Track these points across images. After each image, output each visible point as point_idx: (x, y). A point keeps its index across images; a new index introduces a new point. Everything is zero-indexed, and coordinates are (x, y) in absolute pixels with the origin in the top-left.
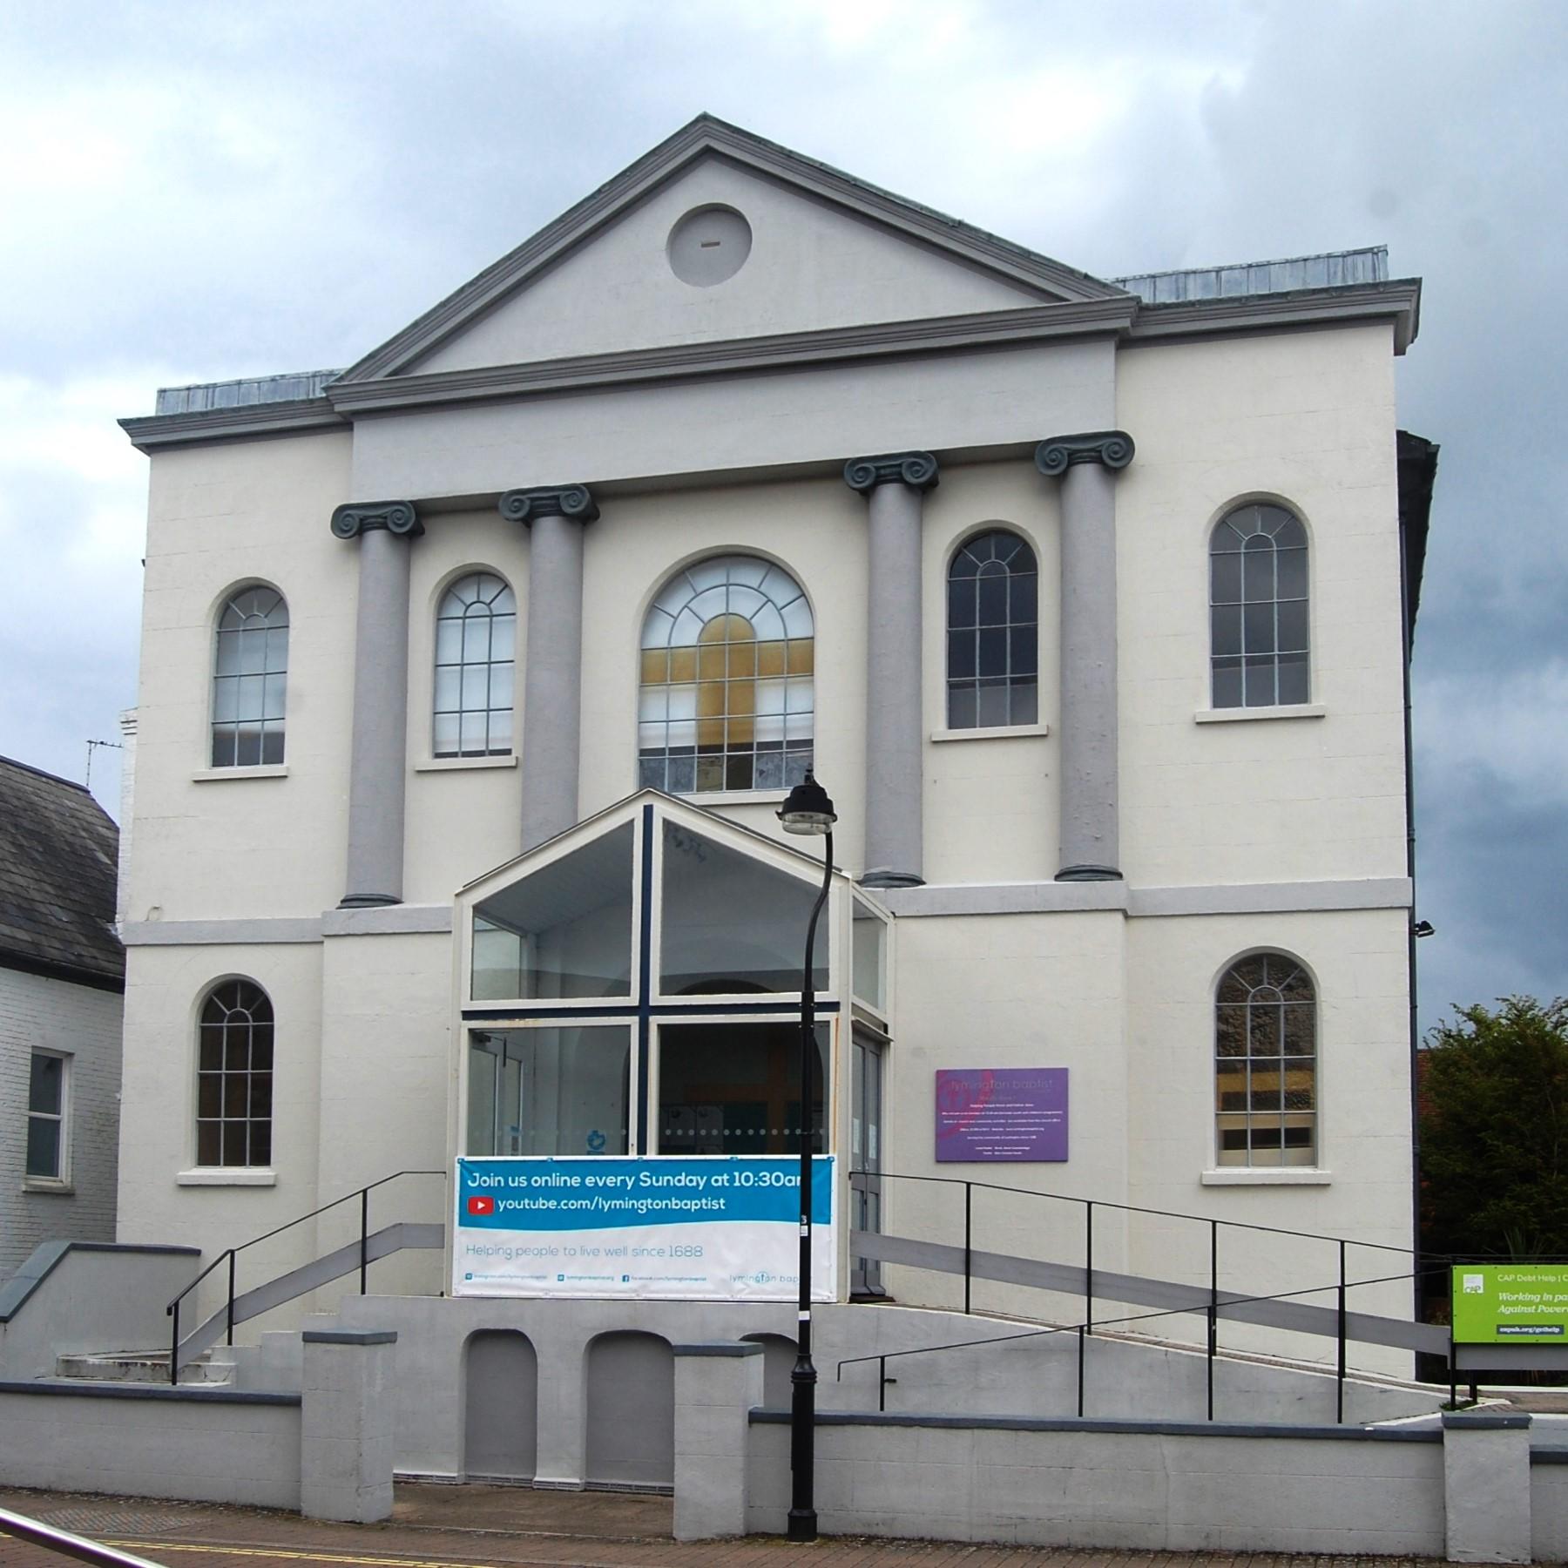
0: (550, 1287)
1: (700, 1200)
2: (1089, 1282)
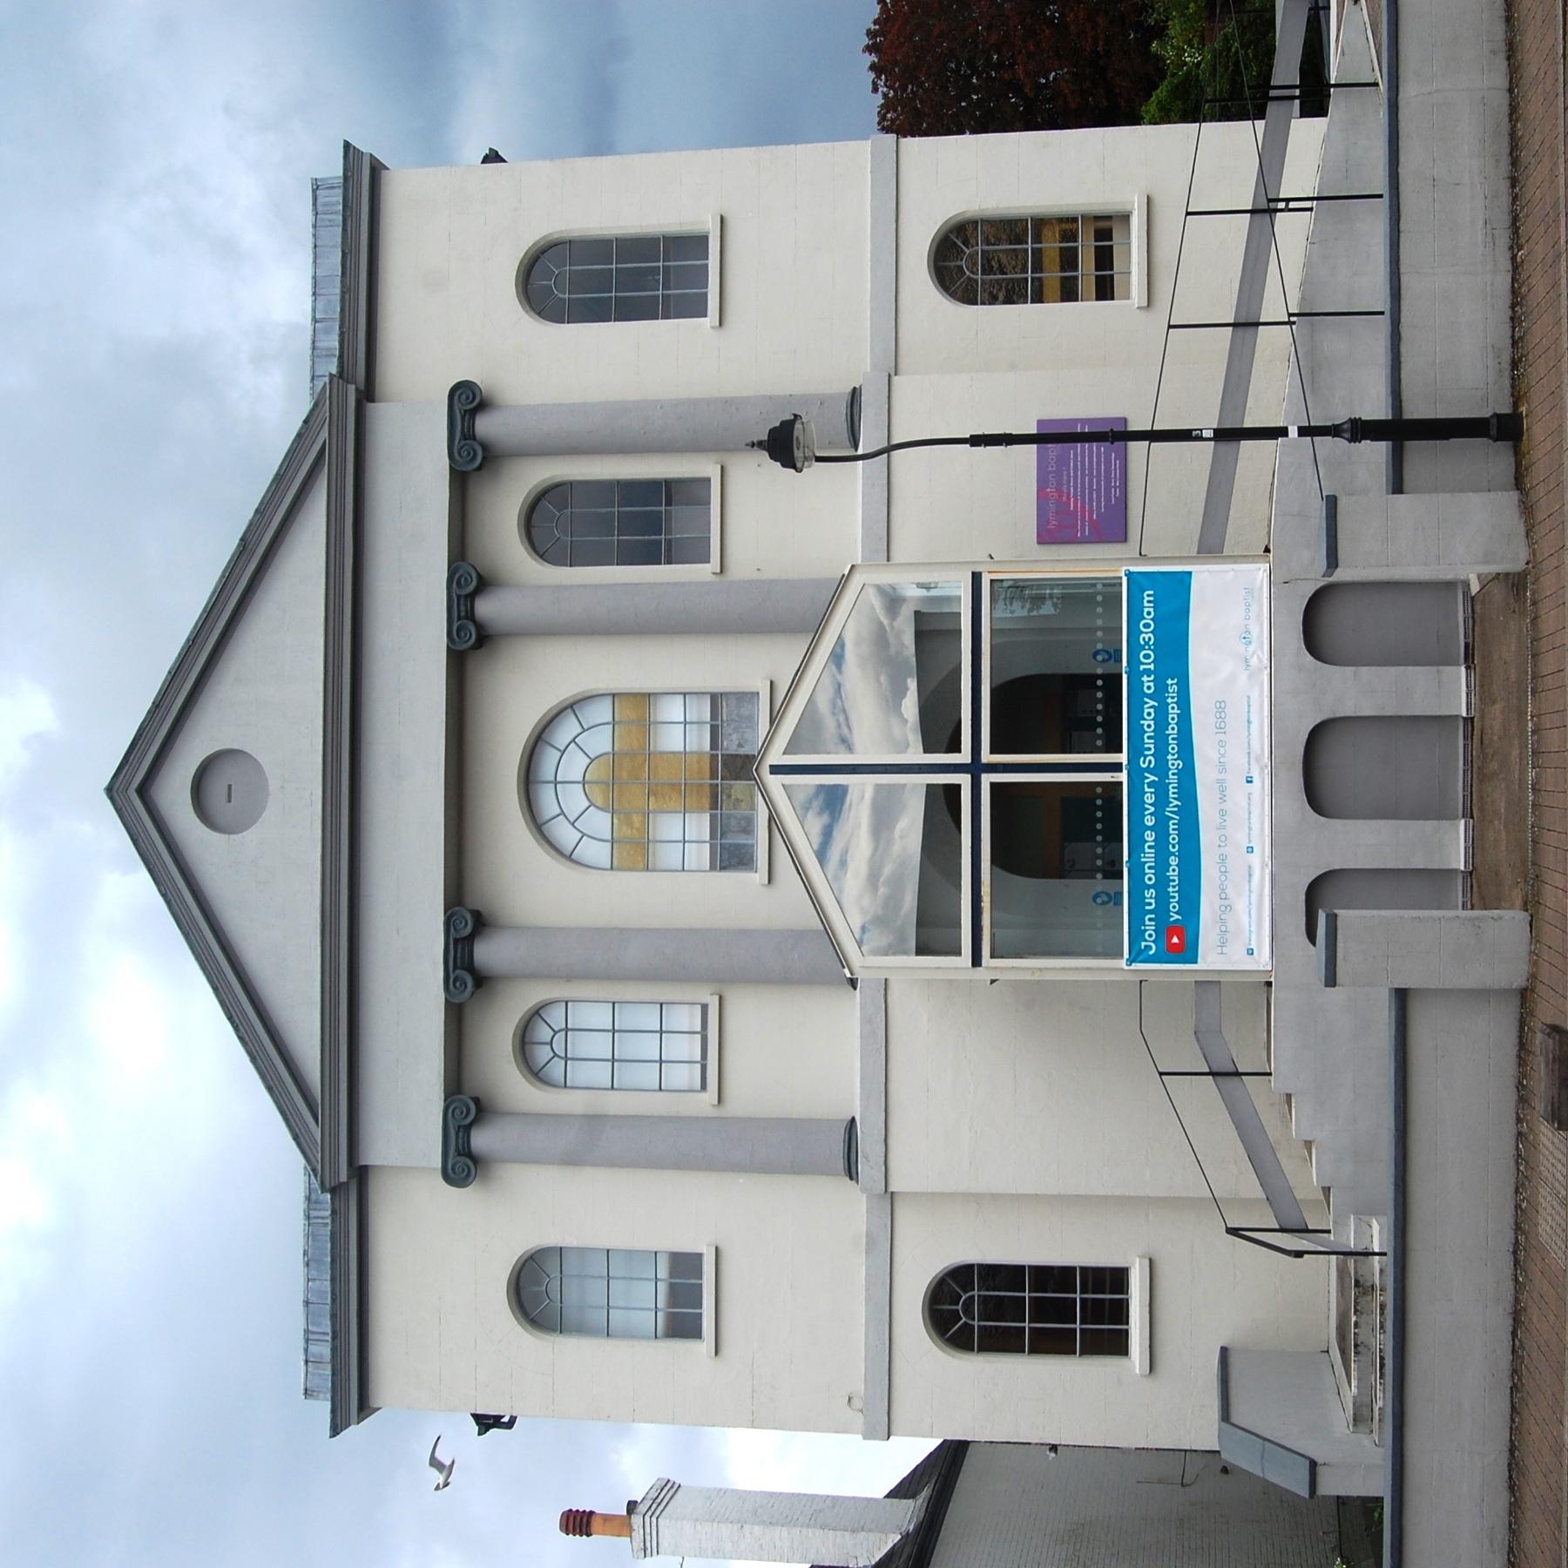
0: (1260, 863)
2: (1246, 325)
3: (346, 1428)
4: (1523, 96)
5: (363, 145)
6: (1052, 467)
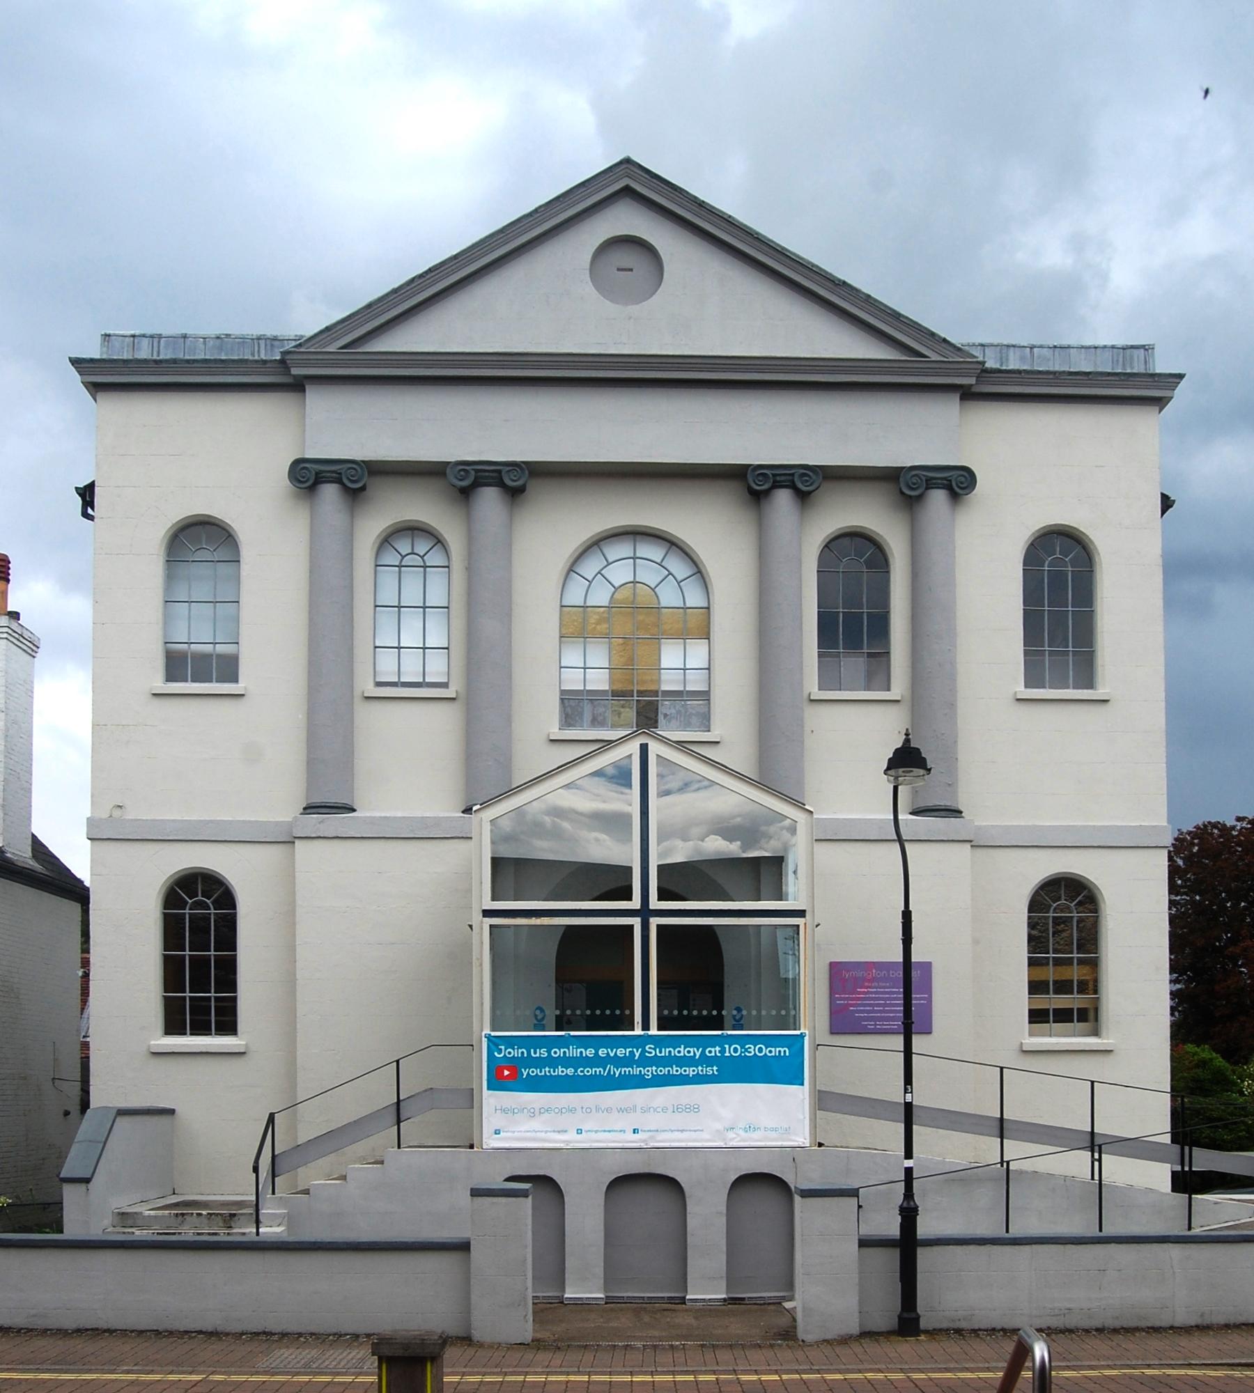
0: (568, 1139)
1: (697, 1067)
2: (1002, 1128)
3: (78, 372)
4: (1166, 1336)
5: (1181, 393)
6: (893, 974)
